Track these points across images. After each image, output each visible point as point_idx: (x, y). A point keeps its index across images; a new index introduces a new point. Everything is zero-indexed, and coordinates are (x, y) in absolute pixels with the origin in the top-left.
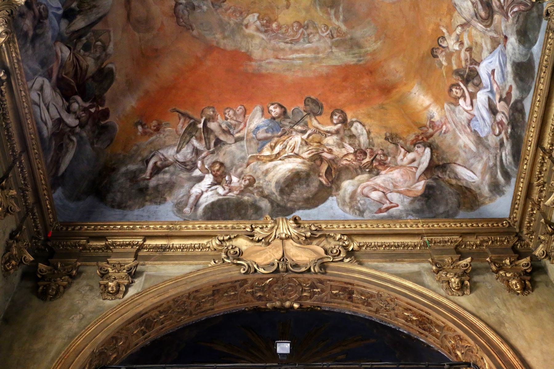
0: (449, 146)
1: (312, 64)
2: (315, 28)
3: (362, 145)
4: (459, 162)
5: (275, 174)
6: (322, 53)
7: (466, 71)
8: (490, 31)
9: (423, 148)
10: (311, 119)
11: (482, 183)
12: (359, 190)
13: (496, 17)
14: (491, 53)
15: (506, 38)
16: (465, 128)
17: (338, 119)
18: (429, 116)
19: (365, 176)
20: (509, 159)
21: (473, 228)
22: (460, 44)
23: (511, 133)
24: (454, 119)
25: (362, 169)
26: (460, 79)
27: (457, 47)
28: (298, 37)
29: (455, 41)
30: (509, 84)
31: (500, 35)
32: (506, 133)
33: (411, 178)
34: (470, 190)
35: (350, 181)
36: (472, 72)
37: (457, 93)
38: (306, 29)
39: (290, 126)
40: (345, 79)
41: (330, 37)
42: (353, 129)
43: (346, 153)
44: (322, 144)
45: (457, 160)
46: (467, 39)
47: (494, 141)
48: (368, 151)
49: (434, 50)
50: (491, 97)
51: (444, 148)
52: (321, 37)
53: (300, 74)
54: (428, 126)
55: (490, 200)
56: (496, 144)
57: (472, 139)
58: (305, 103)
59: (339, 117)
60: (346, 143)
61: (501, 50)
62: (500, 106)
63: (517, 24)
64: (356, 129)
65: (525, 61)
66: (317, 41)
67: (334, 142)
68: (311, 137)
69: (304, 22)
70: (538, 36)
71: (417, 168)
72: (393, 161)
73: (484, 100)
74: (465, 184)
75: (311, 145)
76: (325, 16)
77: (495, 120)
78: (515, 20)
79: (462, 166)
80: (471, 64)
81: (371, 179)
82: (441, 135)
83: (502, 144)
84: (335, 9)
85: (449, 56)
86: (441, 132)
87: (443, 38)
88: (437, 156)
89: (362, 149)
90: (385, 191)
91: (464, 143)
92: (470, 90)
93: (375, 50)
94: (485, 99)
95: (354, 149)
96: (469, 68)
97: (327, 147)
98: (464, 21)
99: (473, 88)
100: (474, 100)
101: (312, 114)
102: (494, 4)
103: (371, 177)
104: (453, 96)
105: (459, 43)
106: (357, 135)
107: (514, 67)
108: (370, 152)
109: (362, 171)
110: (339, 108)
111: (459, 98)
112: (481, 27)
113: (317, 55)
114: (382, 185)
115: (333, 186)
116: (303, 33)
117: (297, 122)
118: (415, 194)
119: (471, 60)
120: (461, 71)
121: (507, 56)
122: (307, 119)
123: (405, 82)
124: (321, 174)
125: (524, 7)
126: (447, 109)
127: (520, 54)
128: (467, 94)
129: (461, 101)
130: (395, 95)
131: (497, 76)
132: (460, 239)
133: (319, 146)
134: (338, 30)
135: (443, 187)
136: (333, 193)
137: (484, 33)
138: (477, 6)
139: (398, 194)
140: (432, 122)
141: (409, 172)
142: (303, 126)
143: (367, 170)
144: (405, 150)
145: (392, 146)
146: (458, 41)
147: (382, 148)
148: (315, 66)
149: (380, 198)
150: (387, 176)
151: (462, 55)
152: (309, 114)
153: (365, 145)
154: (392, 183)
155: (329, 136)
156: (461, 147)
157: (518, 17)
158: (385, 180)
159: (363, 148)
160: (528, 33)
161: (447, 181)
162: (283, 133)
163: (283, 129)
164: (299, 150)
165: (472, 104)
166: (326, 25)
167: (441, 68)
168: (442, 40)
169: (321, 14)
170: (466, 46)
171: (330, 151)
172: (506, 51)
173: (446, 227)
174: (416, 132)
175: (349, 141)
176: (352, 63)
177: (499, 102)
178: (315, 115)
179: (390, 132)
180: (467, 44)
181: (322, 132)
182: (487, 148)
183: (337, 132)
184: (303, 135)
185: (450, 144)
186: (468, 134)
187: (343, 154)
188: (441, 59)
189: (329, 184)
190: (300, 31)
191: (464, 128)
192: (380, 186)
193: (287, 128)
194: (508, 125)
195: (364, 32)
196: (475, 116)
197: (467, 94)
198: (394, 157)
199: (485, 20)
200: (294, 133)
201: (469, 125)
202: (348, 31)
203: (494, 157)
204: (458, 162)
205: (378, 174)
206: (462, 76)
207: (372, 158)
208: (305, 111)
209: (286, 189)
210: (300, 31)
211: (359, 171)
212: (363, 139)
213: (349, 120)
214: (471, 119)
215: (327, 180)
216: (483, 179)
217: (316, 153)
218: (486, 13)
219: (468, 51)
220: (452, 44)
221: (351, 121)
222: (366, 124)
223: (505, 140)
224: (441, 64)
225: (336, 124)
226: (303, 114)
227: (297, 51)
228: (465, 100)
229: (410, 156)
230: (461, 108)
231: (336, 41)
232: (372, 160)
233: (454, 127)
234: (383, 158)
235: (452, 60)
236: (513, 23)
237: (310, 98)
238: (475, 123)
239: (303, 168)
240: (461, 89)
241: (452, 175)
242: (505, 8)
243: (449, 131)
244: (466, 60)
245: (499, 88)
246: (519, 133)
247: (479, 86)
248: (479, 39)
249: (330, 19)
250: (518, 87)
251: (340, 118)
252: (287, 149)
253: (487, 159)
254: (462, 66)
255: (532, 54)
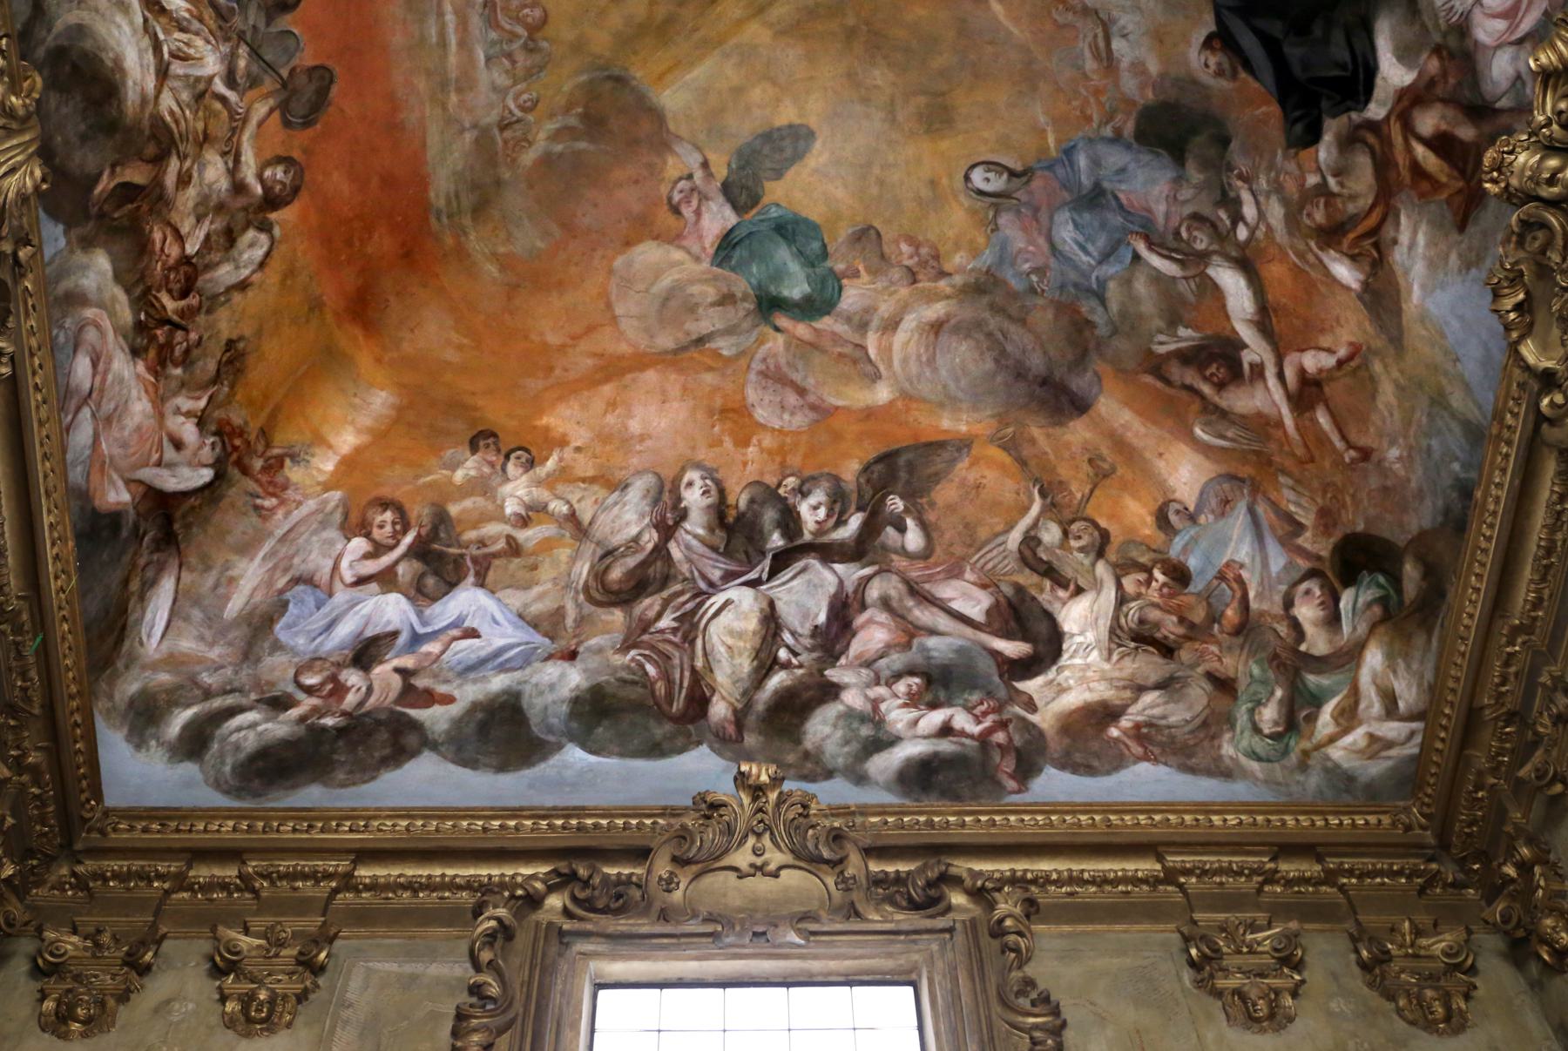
0: (222, 534)
1: (428, 73)
2: (530, 74)
3: (207, 276)
4: (187, 577)
5: (103, 15)
6: (460, 101)
7: (449, 546)
8: (578, 606)
9: (211, 461)
10: (266, 96)
11: (144, 668)
12: (90, 313)
13: (617, 616)
14: (521, 616)
15: (572, 656)
16: (286, 570)
17: (275, 181)
18: (296, 449)
19: (126, 315)
20: (245, 738)
21: (69, 728)
22: (522, 517)
23: (324, 729)
24: (302, 529)
25: (143, 299)
26: (424, 532)
27: (511, 508)
28: (503, 23)
29: (526, 499)
30: (456, 693)
31: (575, 637)
32: (315, 710)
33: (134, 458)
34: (120, 640)
35: (110, 274)
36: (451, 567)
37: (381, 527)
38: (525, 47)
39: (244, 32)
40: (388, 181)
41: (503, 118)
42: (251, 234)
43: (184, 230)
44: (201, 146)
45: (191, 570)
46: (540, 536)
47: (277, 673)
48: (193, 300)
49: (490, 441)
50: (402, 639)
51: (217, 518)
52: (502, 92)
53: (397, 40)
54: (268, 454)
55: (108, 710)
56: (272, 684)
57: (258, 598)
58: (315, 68)
59: (281, 182)
60: (212, 223)
61: (536, 648)
62: (384, 672)
63: (617, 684)
64: (252, 245)
65: (535, 729)
66: (493, 83)
67: (210, 186)
68: (218, 106)
69: (545, 39)
70: (610, 754)
71: (159, 464)
72: (174, 384)
73: (385, 619)
74: (132, 618)
75: (197, 112)
76: (561, 100)
77: (339, 666)
78: (624, 675)
79: (176, 592)
80: (475, 560)
81: (121, 339)
82: (248, 498)
83: (279, 704)
84: (581, 127)
85: (481, 486)
86: (258, 497)
87: (530, 464)
88: (193, 508)
89: (196, 279)
90: (94, 395)
91: (241, 576)
92: (401, 569)
93: (469, 256)
94: (389, 622)
95: (197, 253)
96: (462, 556)
97: (196, 167)
98: (586, 518)
99: (408, 578)
100: (374, 586)
101: (283, 95)
102: (647, 601)
103: (125, 337)
104: (370, 514)
105: (523, 513)
106: (235, 252)
107: (505, 697)
108: (189, 307)
109: (139, 299)
110: (307, 178)
111: (368, 536)
112: (580, 574)
113: (452, 88)
114: (110, 377)
115: (91, 224)
116: (514, 36)
117: (259, 52)
118: (95, 490)
119: (486, 556)
120: (448, 532)
121: (528, 671)
122: (269, 84)
123: (386, 359)
124: (118, 169)
125: (663, 692)
126: (325, 502)
127: (546, 708)
128: (386, 560)
129: (359, 544)
130: (348, 337)
131: (465, 649)
132: (37, 711)
133: (196, 140)
134: (526, 141)
135: (119, 560)
136: (74, 233)
137: (567, 586)
138: (634, 553)
139: (90, 441)
140: (280, 462)
141: (148, 446)
142: (249, 75)
143: (143, 317)
144: (204, 411)
145: (211, 366)
146: (529, 508)
147: (205, 337)
148: (421, 84)
149: (78, 390)
150: (133, 383)
151: (492, 529)
152: (284, 85)
153: (209, 285)
154: (115, 409)
155: (226, 163)
156: (227, 569)
157: (634, 683)
158: (121, 381)
159: (199, 283)
160: (606, 723)
161: (134, 565)
162: (224, 12)
163: (233, 8)
164: (178, 77)
165: (361, 581)
166: (536, 103)
167: (445, 466)
168: (523, 460)
169: (566, 88)
170: (522, 535)
171: (184, 180)
172: (537, 665)
173: (65, 656)
174: (251, 425)
175: (215, 230)
176: (432, 194)
177: (397, 670)
178: (284, 107)
179: (248, 350)
180: (527, 539)
181: (235, 139)
182: (248, 654)
183: (239, 187)
184: (222, 80)
185: (229, 532)
186: (269, 583)
187: (179, 225)
188: (469, 464)
189: (96, 209)
190: (520, 30)
191: (282, 565)
192: (106, 372)
193: (237, 21)
194: (344, 714)
195: (520, 218)
196: (331, 595)
197: (386, 560)
198: (183, 385)
199: (603, 586)
200: (225, 48)
201: (297, 581)
202: (520, 171)
203: (230, 682)
204: (184, 574)
205: (135, 352)
206: (434, 534)
207: (175, 318)
208: (292, 71)
209: (67, 68)
210: (520, 30)
211: (138, 291)
212: (225, 274)
213: (273, 216)
214: (317, 586)
215: (105, 195)
216: (155, 666)
217: (177, 136)
218: (620, 581)
219: (508, 543)
220: (519, 493)
221: (271, 224)
222: (267, 270)
223: (294, 713)
224: (454, 467)
225: (260, 177)
226: (282, 67)
227: (463, 24)
228: (367, 556)
229: (189, 432)
230: (339, 546)
231: (493, 140)
232: (169, 322)
233: (279, 532)
234: (178, 351)
235: (473, 499)
236: (615, 669)
237: (331, 81)
238: (310, 601)
239: (129, 103)
240: (397, 537)
241: (150, 574)
242: (646, 637)
243: (265, 519)
244: (482, 543)
245: (435, 661)
246: (336, 757)
247: (421, 595)
248: (546, 573)
249: (552, 116)
250: (458, 723)
251: (278, 188)
252: (178, 35)
253: (214, 661)
254: (463, 531)
255: (560, 747)
